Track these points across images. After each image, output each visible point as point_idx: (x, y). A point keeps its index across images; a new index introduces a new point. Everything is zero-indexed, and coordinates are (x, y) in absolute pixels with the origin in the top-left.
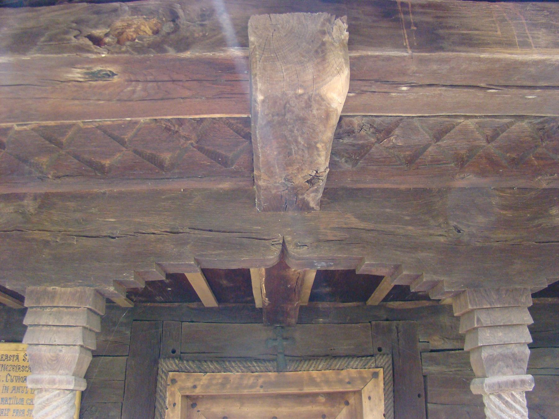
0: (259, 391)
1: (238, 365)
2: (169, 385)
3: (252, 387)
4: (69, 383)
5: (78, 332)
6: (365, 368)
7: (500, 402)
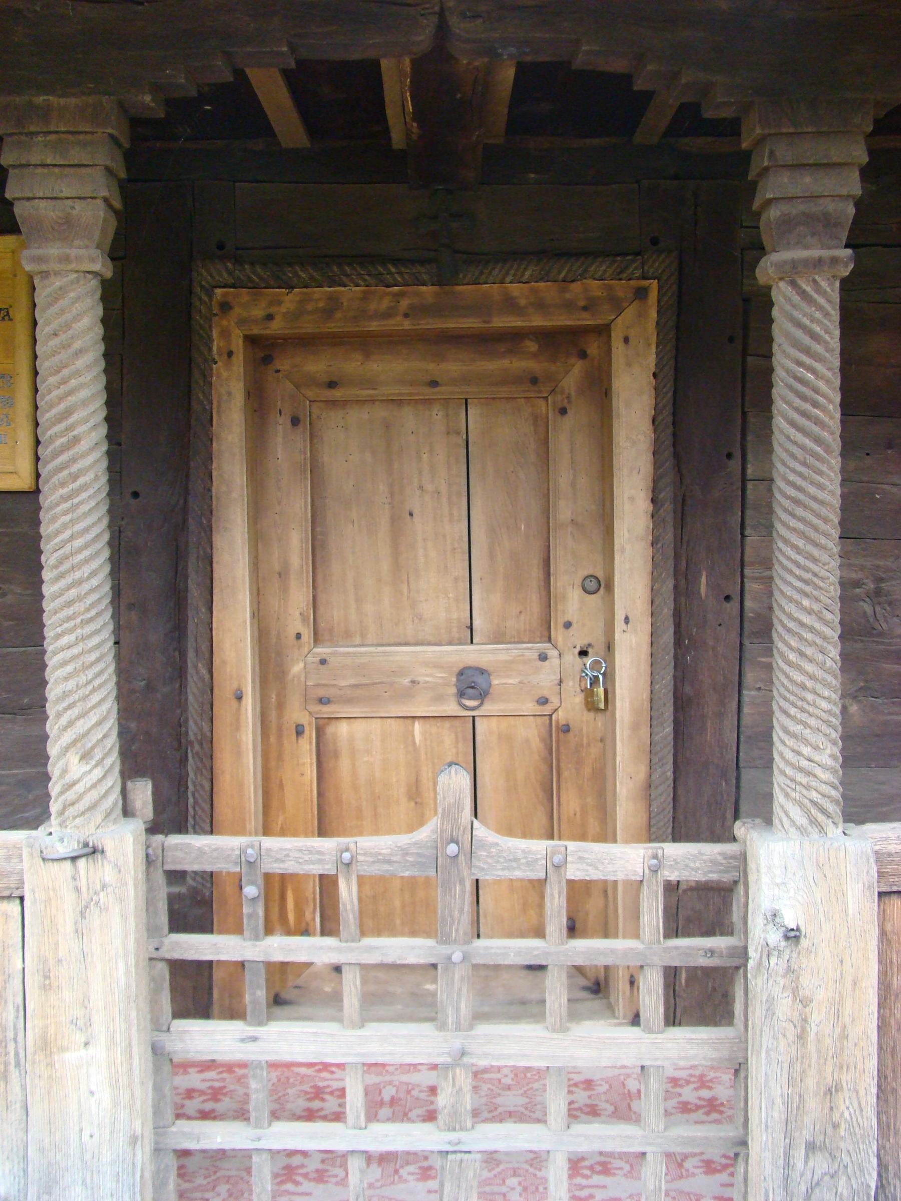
0: (402, 325)
1: (356, 271)
2: (216, 315)
3: (388, 314)
4: (93, 260)
5: (98, 175)
6: (621, 279)
7: (794, 292)
